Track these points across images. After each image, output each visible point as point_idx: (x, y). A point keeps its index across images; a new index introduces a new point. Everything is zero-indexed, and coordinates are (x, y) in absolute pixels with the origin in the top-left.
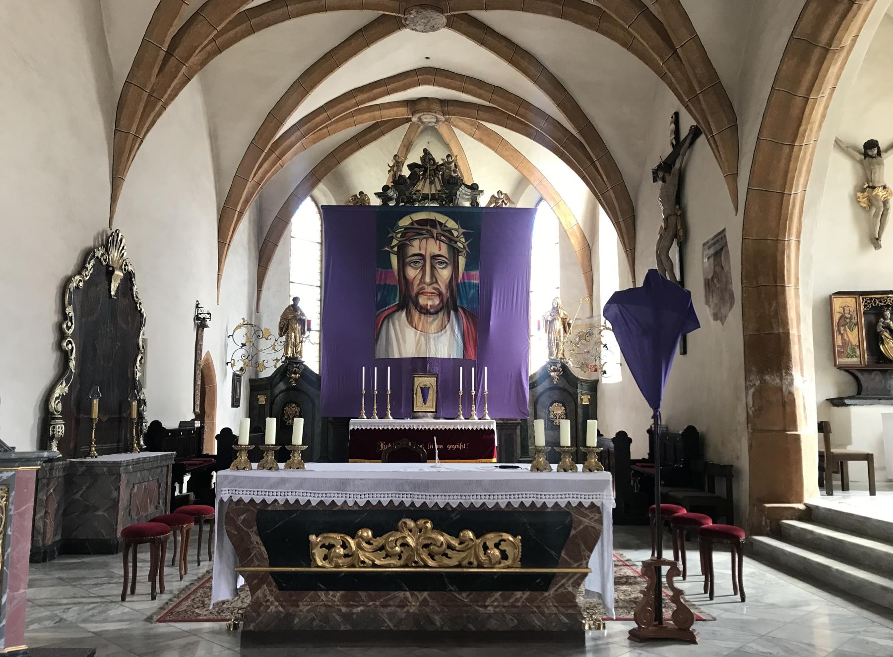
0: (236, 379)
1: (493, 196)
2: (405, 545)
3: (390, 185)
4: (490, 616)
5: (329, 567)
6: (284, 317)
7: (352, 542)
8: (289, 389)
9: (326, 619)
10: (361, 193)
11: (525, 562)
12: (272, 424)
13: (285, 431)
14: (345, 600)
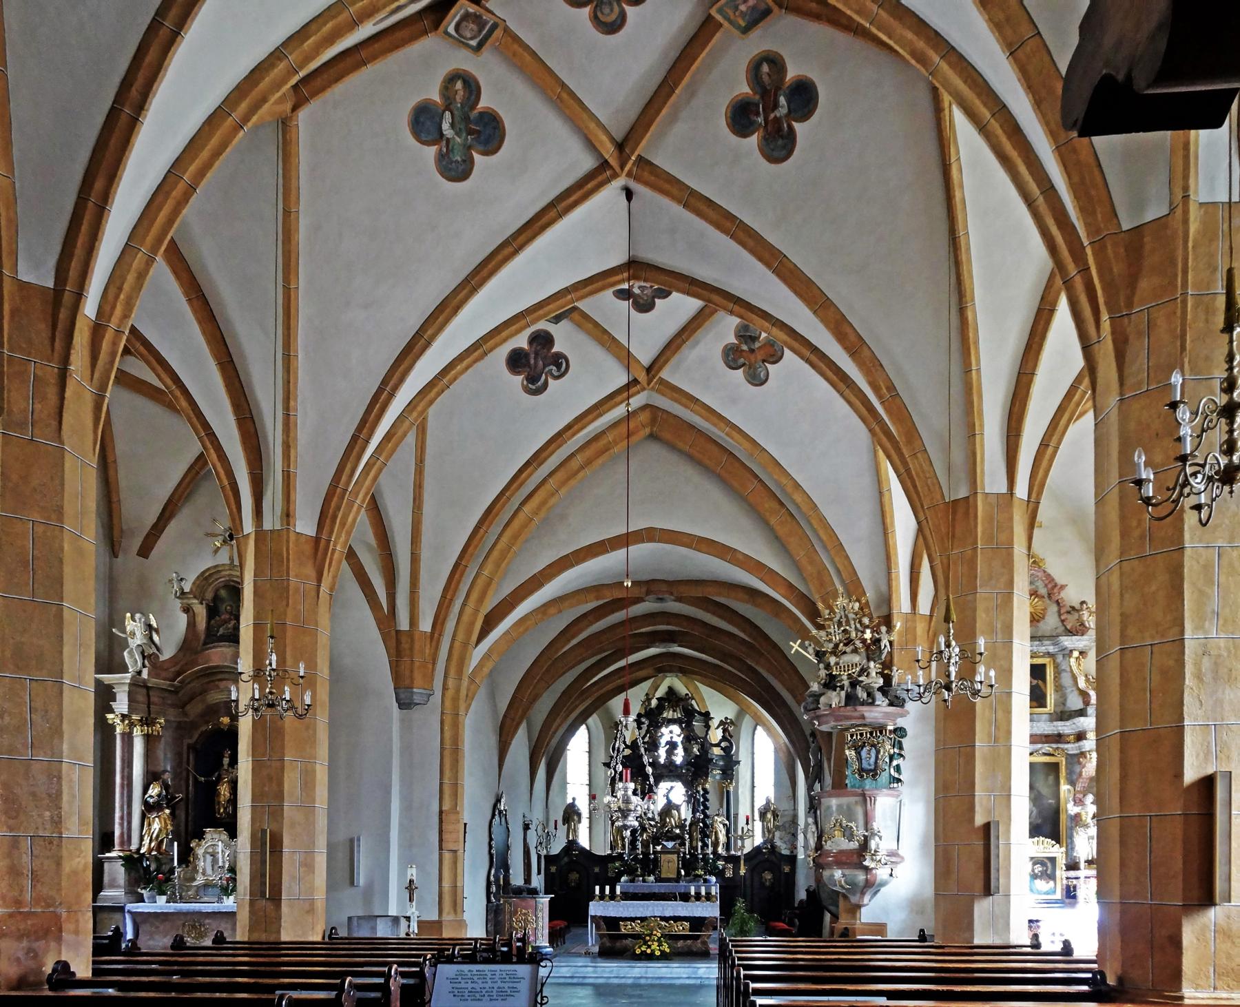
3: (643, 712)
5: (626, 932)
6: (565, 812)
8: (571, 861)
12: (607, 888)
13: (602, 890)
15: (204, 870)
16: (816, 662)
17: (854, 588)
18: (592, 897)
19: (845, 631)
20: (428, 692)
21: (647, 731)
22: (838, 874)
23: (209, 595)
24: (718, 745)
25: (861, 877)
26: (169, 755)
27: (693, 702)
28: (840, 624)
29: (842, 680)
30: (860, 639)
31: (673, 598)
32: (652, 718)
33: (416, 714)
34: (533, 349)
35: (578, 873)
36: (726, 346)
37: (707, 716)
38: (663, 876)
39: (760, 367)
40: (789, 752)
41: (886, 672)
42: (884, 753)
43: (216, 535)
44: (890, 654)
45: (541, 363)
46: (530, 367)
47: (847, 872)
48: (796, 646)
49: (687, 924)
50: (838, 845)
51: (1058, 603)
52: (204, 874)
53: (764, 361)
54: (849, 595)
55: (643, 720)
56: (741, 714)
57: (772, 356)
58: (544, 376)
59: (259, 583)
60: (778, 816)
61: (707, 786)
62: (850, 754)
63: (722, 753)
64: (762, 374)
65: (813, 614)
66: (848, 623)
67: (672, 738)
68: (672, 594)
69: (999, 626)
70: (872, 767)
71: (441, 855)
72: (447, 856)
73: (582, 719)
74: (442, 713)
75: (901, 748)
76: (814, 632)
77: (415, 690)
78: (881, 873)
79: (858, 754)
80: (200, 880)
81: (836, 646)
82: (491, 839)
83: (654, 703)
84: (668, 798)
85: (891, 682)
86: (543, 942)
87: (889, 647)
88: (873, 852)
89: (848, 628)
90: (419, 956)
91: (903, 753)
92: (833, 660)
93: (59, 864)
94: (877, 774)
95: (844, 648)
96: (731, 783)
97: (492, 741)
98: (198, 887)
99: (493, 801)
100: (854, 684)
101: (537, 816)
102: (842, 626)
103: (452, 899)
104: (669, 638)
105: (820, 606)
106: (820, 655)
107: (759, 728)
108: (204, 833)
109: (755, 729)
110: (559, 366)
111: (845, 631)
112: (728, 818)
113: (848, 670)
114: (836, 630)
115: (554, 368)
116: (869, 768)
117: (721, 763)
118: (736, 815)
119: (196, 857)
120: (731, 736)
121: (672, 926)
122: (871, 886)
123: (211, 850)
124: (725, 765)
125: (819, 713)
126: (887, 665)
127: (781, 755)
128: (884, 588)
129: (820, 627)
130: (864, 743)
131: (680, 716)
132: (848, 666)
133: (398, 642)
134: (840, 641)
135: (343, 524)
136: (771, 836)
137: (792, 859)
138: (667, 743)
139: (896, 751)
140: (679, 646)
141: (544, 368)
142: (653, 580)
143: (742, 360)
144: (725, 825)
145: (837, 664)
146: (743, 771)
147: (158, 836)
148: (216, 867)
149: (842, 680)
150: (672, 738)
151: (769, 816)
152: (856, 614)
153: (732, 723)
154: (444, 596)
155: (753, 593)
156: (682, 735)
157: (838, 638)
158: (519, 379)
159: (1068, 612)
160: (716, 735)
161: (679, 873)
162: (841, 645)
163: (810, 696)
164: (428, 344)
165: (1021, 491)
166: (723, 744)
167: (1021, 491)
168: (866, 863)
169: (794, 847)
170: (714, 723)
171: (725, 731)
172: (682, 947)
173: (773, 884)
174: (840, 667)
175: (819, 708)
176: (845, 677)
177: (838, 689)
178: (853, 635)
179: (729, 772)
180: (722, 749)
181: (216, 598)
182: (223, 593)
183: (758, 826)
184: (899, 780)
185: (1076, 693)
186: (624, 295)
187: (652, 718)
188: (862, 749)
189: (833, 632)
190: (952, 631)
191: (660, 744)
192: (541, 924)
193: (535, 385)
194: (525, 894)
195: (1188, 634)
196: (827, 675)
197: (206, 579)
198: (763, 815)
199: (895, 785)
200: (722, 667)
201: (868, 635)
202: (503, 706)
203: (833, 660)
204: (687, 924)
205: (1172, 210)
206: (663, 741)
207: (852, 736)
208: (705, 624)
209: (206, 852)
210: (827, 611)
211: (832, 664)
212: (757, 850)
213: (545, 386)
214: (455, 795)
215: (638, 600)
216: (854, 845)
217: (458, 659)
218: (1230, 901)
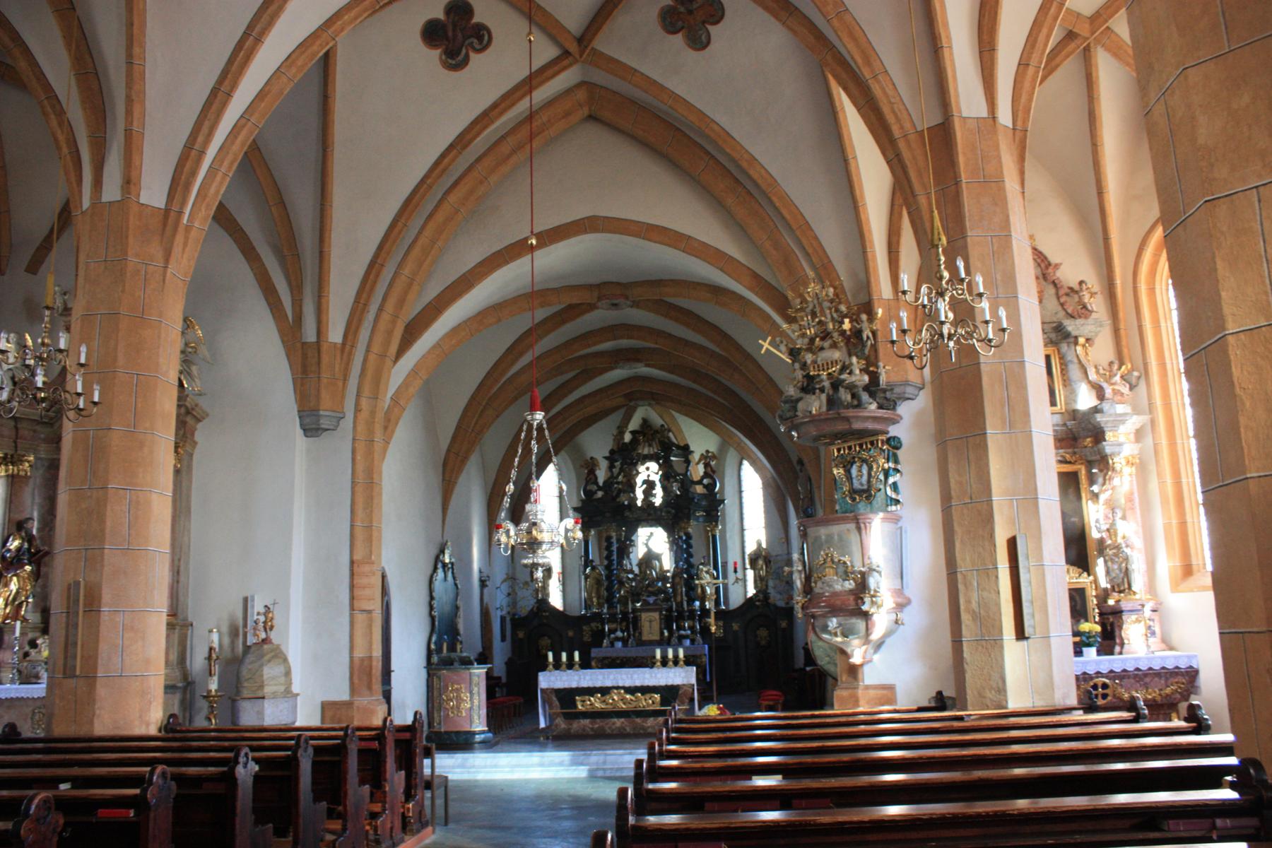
0: (503, 619)
1: (702, 455)
2: (613, 700)
3: (615, 448)
4: (649, 727)
7: (592, 699)
9: (584, 730)
10: (592, 458)
11: (662, 705)
13: (570, 657)
14: (591, 723)
16: (790, 361)
17: (825, 271)
18: (544, 667)
19: (820, 322)
20: (338, 415)
21: (621, 470)
26: (37, 500)
27: (671, 435)
28: (814, 314)
29: (822, 381)
30: (838, 331)
31: (628, 303)
34: (450, 20)
35: (550, 637)
36: (662, 9)
37: (685, 451)
38: (645, 638)
39: (700, 30)
40: (778, 487)
41: (871, 369)
42: (878, 468)
45: (460, 35)
46: (447, 39)
49: (657, 696)
50: (830, 586)
51: (1054, 283)
54: (821, 280)
56: (723, 448)
57: (712, 16)
58: (464, 51)
60: (770, 562)
62: (838, 472)
64: (703, 37)
65: (782, 305)
67: (649, 476)
68: (627, 298)
69: (999, 277)
70: (865, 487)
71: (352, 616)
74: (354, 439)
75: (896, 461)
76: (785, 326)
77: (321, 413)
79: (848, 472)
81: (812, 340)
82: (432, 598)
83: (627, 437)
84: (647, 545)
85: (879, 381)
86: (479, 724)
87: (872, 338)
88: (872, 593)
89: (823, 319)
91: (899, 467)
92: (809, 358)
94: (871, 495)
95: (821, 343)
96: (717, 525)
97: (436, 480)
99: (434, 552)
100: (836, 384)
102: (816, 317)
105: (790, 294)
106: (794, 353)
107: (745, 463)
109: (741, 464)
110: (480, 38)
111: (820, 322)
112: (716, 568)
113: (828, 369)
114: (810, 322)
115: (475, 41)
116: (860, 487)
117: (704, 503)
118: (725, 564)
120: (714, 472)
121: (638, 700)
125: (797, 421)
128: (862, 276)
129: (791, 320)
130: (854, 458)
131: (656, 451)
132: (827, 364)
133: (305, 356)
134: (817, 336)
136: (764, 583)
137: (789, 612)
138: (645, 482)
139: (891, 465)
140: (647, 365)
141: (464, 42)
142: (605, 283)
143: (680, 24)
145: (814, 362)
147: (15, 599)
149: (822, 381)
150: (649, 476)
151: (760, 562)
152: (832, 301)
153: (714, 457)
154: (357, 300)
155: (717, 292)
156: (660, 473)
157: (813, 332)
158: (436, 53)
159: (1067, 295)
160: (698, 471)
161: (662, 633)
162: (818, 339)
163: (785, 402)
165: (1005, 116)
166: (705, 481)
167: (1005, 116)
168: (865, 608)
171: (707, 465)
172: (652, 727)
174: (818, 366)
175: (797, 416)
177: (818, 391)
178: (831, 326)
179: (714, 513)
180: (705, 486)
184: (897, 502)
187: (626, 458)
188: (852, 465)
189: (806, 324)
190: (943, 259)
191: (636, 483)
192: (476, 702)
193: (455, 59)
196: (804, 377)
199: (894, 508)
201: (847, 325)
203: (809, 358)
204: (657, 696)
206: (639, 480)
207: (839, 450)
210: (798, 301)
211: (809, 362)
212: (749, 602)
213: (466, 61)
215: (592, 307)
216: (850, 585)
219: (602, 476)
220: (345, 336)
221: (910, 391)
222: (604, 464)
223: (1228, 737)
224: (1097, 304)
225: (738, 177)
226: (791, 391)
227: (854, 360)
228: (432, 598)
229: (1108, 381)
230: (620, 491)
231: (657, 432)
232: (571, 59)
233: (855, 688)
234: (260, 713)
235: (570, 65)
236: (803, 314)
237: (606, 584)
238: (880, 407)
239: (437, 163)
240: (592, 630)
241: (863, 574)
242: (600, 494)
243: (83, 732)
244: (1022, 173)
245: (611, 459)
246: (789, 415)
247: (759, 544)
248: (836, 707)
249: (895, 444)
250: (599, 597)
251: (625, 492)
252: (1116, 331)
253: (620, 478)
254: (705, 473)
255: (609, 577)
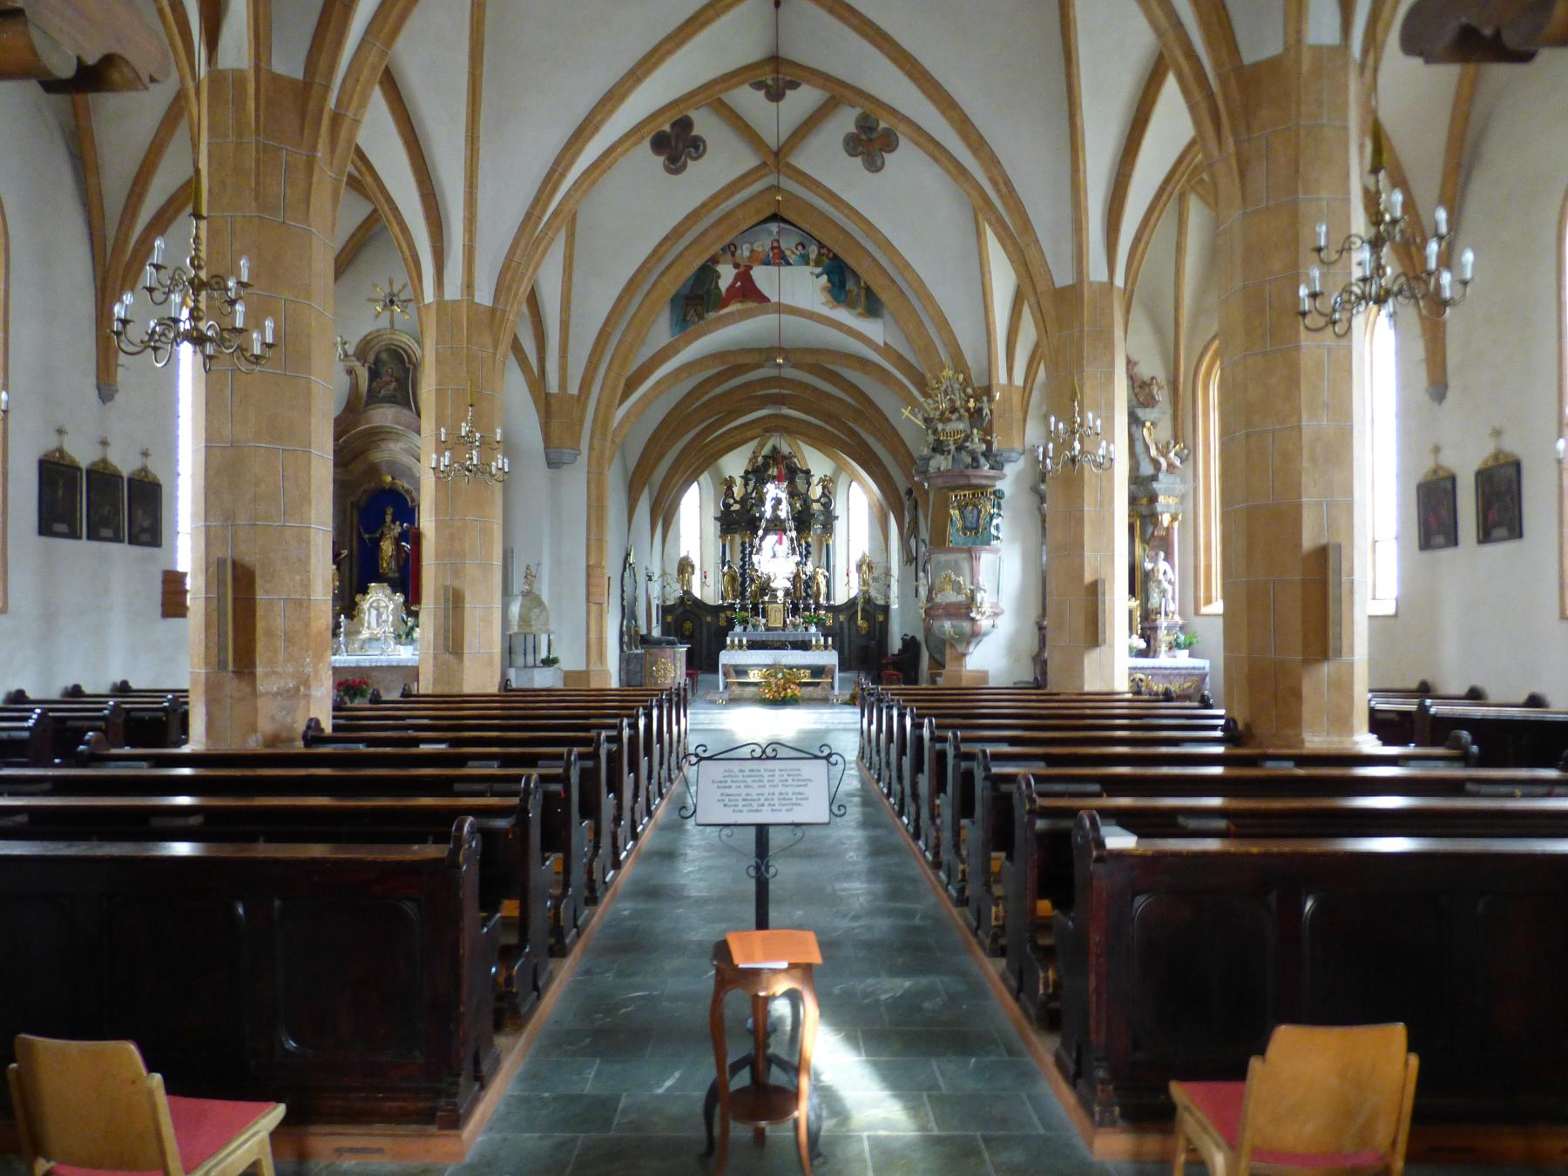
0: (658, 605)
8: (686, 611)
15: (369, 624)
18: (724, 647)
19: (950, 399)
21: (755, 487)
22: (947, 625)
23: (371, 358)
24: (818, 501)
25: (966, 625)
27: (796, 460)
28: (946, 393)
32: (758, 474)
33: (565, 472)
37: (808, 472)
43: (377, 301)
44: (991, 422)
45: (681, 146)
47: (955, 623)
48: (906, 412)
52: (369, 628)
53: (881, 150)
55: (750, 476)
57: (888, 146)
58: (683, 158)
59: (441, 351)
61: (810, 539)
63: (822, 508)
65: (922, 384)
66: (953, 393)
69: (1103, 402)
72: (594, 608)
73: (693, 477)
75: (999, 507)
78: (984, 623)
79: (962, 513)
80: (365, 634)
82: (623, 591)
83: (760, 459)
90: (632, 708)
91: (1002, 513)
93: (307, 625)
98: (364, 641)
99: (624, 555)
100: (960, 448)
101: (656, 570)
103: (595, 648)
104: (779, 400)
105: (929, 376)
106: (927, 420)
107: (854, 484)
108: (368, 588)
109: (850, 486)
110: (697, 148)
112: (828, 570)
117: (822, 518)
119: (362, 611)
122: (975, 635)
123: (375, 604)
124: (826, 520)
126: (988, 431)
127: (875, 510)
129: (926, 395)
135: (516, 295)
137: (886, 609)
139: (996, 510)
144: (825, 576)
145: (943, 430)
146: (839, 526)
148: (380, 621)
154: (590, 361)
160: (816, 492)
164: (597, 129)
165: (1119, 281)
167: (1119, 281)
168: (972, 615)
169: (887, 597)
170: (815, 480)
171: (824, 488)
173: (868, 632)
176: (951, 443)
178: (958, 404)
181: (377, 361)
182: (384, 356)
183: (854, 576)
184: (998, 538)
185: (1147, 460)
186: (758, 85)
192: (678, 672)
193: (675, 164)
194: (664, 645)
195: (1304, 423)
197: (369, 342)
198: (859, 567)
200: (825, 429)
201: (972, 404)
202: (632, 465)
203: (940, 427)
205: (1287, 50)
206: (769, 497)
207: (956, 497)
208: (815, 389)
209: (371, 606)
210: (934, 382)
213: (684, 166)
214: (600, 550)
217: (602, 419)
218: (1341, 656)
219: (738, 491)
220: (581, 389)
221: (1014, 455)
222: (739, 481)
223: (1221, 712)
224: (1162, 396)
225: (894, 278)
226: (926, 451)
227: (975, 431)
228: (623, 591)
229: (1165, 456)
230: (753, 505)
231: (784, 457)
232: (767, 169)
233: (1328, 733)
234: (531, 679)
235: (766, 175)
236: (937, 392)
237: (740, 579)
238: (992, 468)
239: (655, 251)
240: (727, 617)
241: (972, 591)
242: (736, 507)
243: (455, 691)
244: (1126, 323)
245: (746, 478)
246: (923, 470)
247: (864, 554)
248: (842, 675)
249: (999, 495)
250: (734, 590)
251: (757, 506)
252: (1175, 417)
253: (754, 495)
254: (823, 493)
255: (742, 575)
